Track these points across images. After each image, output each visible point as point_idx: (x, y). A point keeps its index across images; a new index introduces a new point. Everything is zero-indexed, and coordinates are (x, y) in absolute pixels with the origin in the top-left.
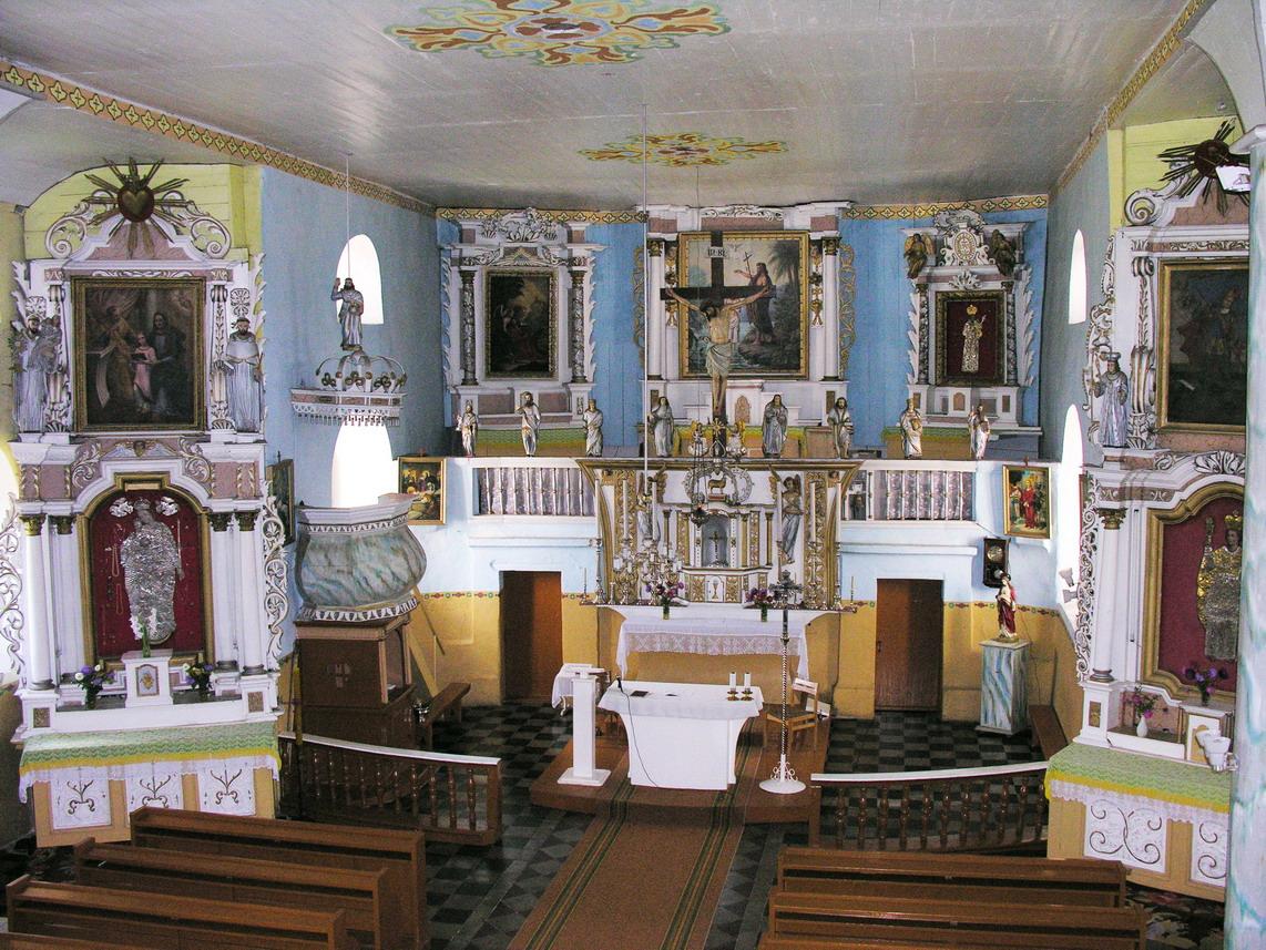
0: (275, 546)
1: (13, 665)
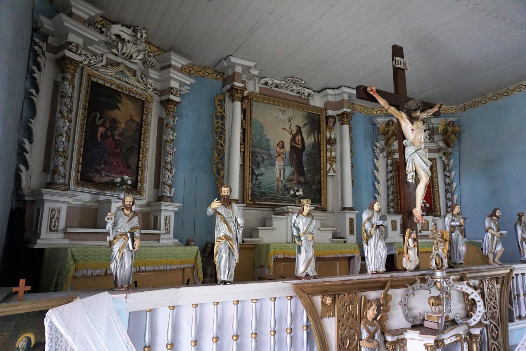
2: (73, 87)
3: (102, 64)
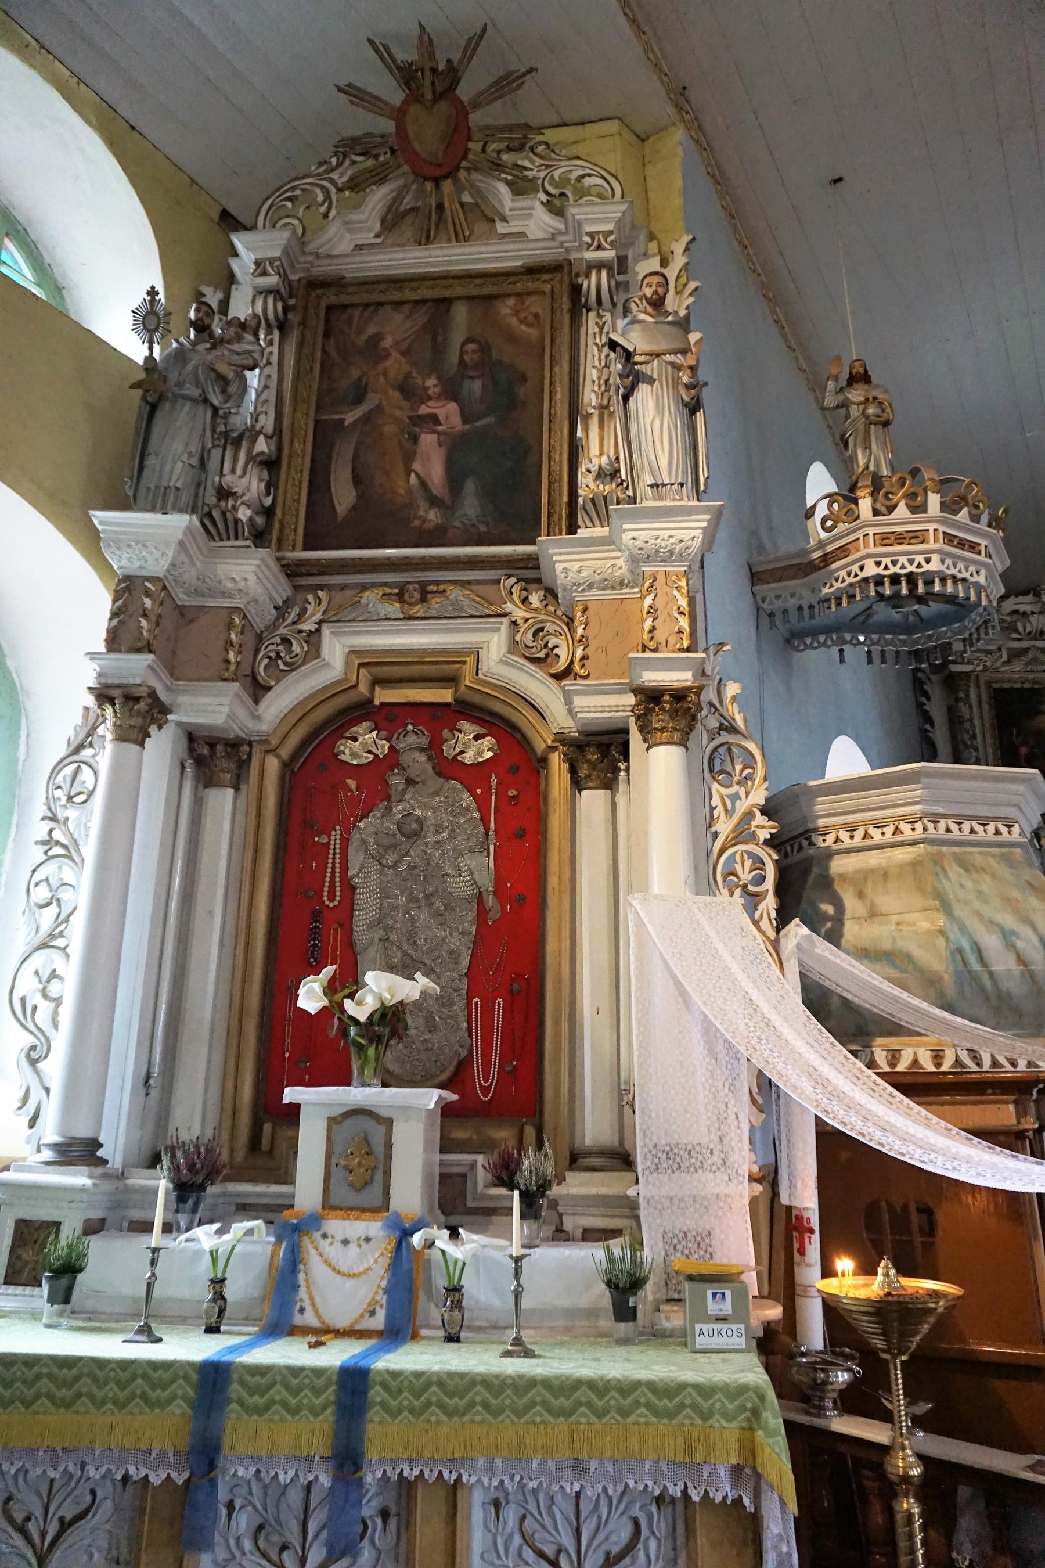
0: (742, 807)
1: (25, 1100)
2: (971, 706)
3: (1003, 660)
